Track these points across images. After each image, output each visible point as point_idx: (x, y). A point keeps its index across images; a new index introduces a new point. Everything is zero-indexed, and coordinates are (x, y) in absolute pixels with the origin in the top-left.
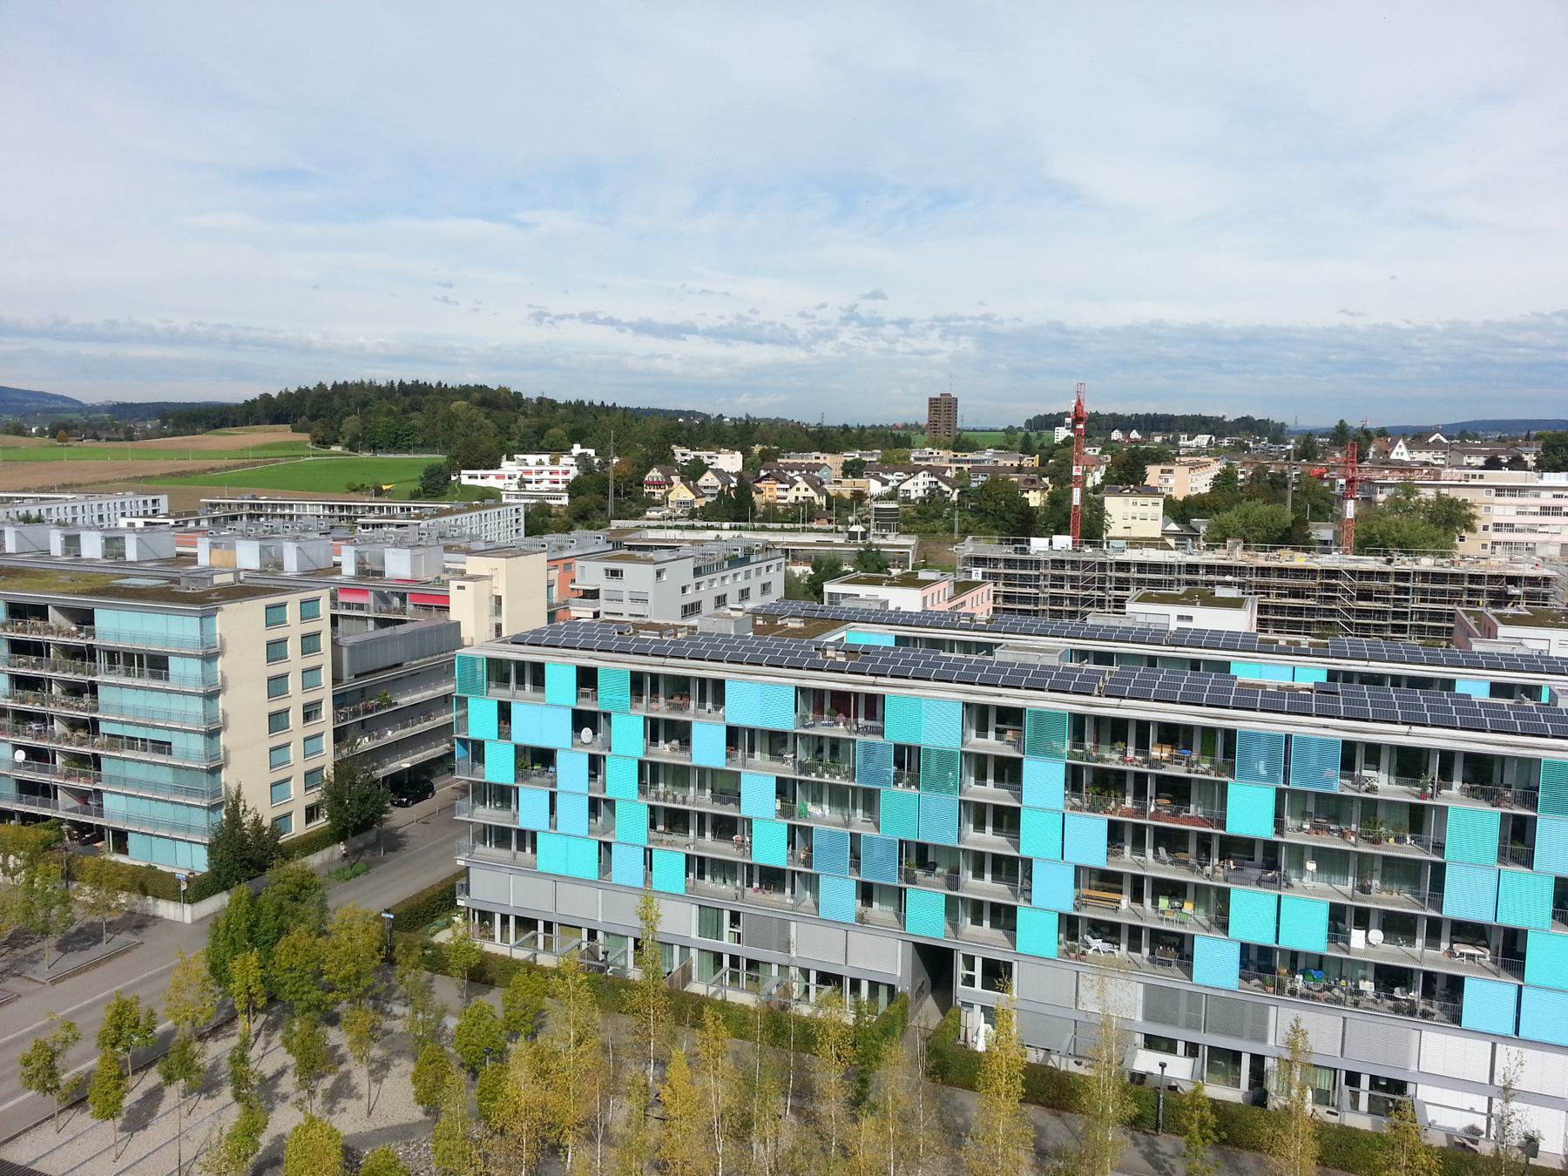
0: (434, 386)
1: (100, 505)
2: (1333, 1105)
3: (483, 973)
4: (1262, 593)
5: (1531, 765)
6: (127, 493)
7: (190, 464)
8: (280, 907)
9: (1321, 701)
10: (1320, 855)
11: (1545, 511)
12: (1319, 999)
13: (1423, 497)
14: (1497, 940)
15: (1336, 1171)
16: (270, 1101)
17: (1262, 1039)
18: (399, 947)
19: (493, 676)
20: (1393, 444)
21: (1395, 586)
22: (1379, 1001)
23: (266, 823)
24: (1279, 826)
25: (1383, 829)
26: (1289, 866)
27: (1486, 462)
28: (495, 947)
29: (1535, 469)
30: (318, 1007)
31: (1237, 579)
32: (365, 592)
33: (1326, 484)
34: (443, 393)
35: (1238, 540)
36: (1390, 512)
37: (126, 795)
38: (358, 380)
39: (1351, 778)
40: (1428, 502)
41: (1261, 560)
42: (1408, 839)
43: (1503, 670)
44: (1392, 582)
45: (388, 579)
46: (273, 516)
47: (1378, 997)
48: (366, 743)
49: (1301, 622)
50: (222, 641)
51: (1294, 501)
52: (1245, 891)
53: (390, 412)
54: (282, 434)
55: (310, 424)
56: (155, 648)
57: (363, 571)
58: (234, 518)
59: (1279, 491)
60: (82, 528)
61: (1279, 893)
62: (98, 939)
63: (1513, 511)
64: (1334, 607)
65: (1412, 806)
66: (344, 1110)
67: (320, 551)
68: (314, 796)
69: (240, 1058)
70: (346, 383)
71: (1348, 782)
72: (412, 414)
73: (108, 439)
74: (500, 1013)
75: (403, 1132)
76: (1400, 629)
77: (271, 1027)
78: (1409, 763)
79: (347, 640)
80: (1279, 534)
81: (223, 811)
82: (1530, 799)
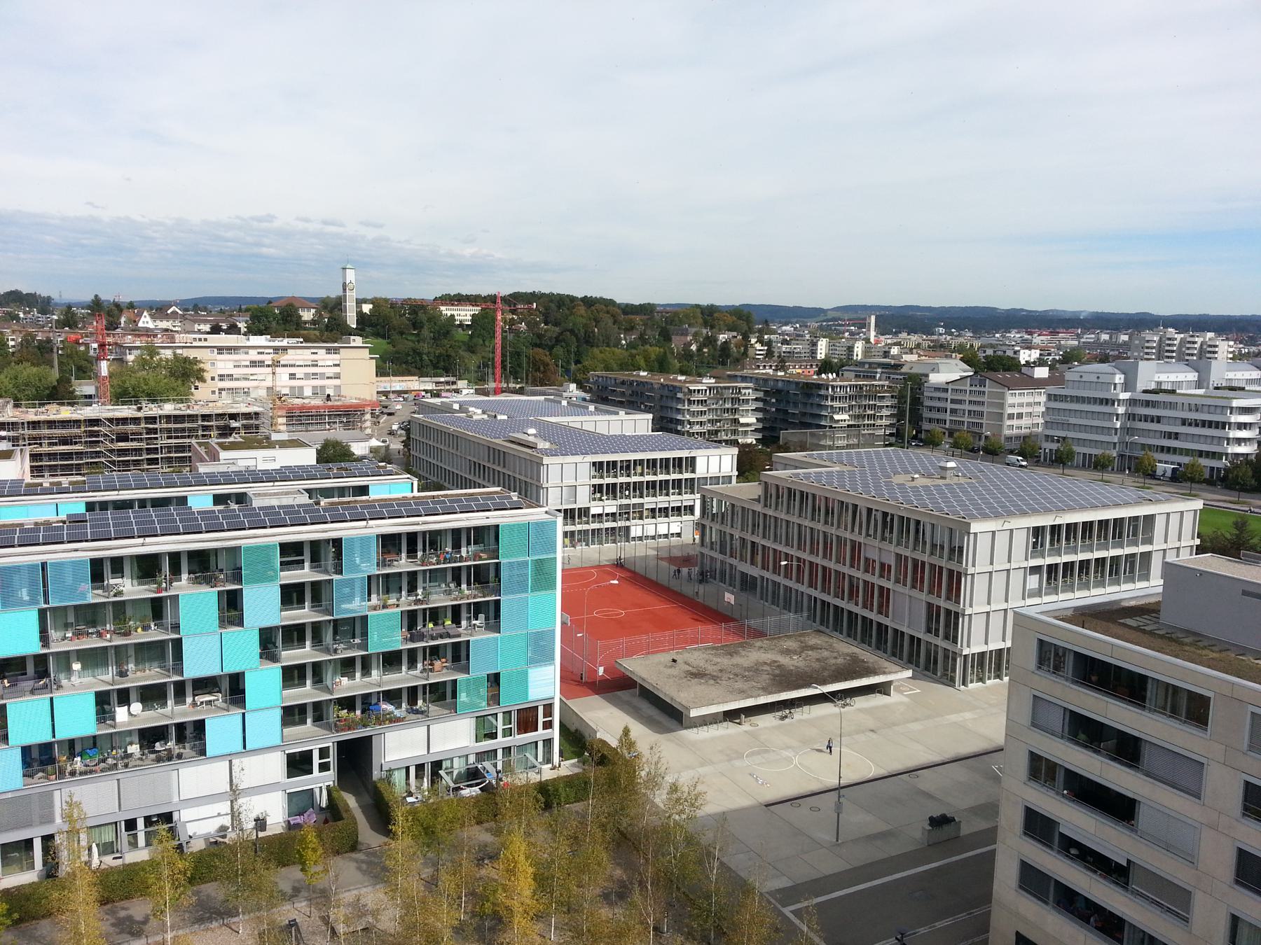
2: (117, 851)
4: (35, 444)
5: (235, 551)
9: (74, 529)
10: (84, 656)
11: (254, 364)
12: (96, 772)
13: (163, 356)
14: (225, 685)
15: (123, 902)
17: (49, 819)
20: (140, 315)
21: (146, 428)
22: (144, 757)
24: (44, 639)
25: (131, 623)
26: (58, 671)
27: (211, 328)
29: (245, 334)
31: (11, 434)
33: (82, 348)
35: (8, 399)
36: (139, 369)
39: (102, 587)
40: (167, 361)
41: (32, 415)
42: (152, 626)
43: (318, 479)
44: (143, 425)
47: (143, 755)
49: (72, 465)
51: (60, 363)
52: (21, 702)
59: (47, 355)
61: (51, 695)
63: (231, 365)
64: (98, 449)
65: (153, 600)
71: (100, 592)
76: (154, 461)
78: (147, 567)
80: (47, 392)
82: (237, 577)
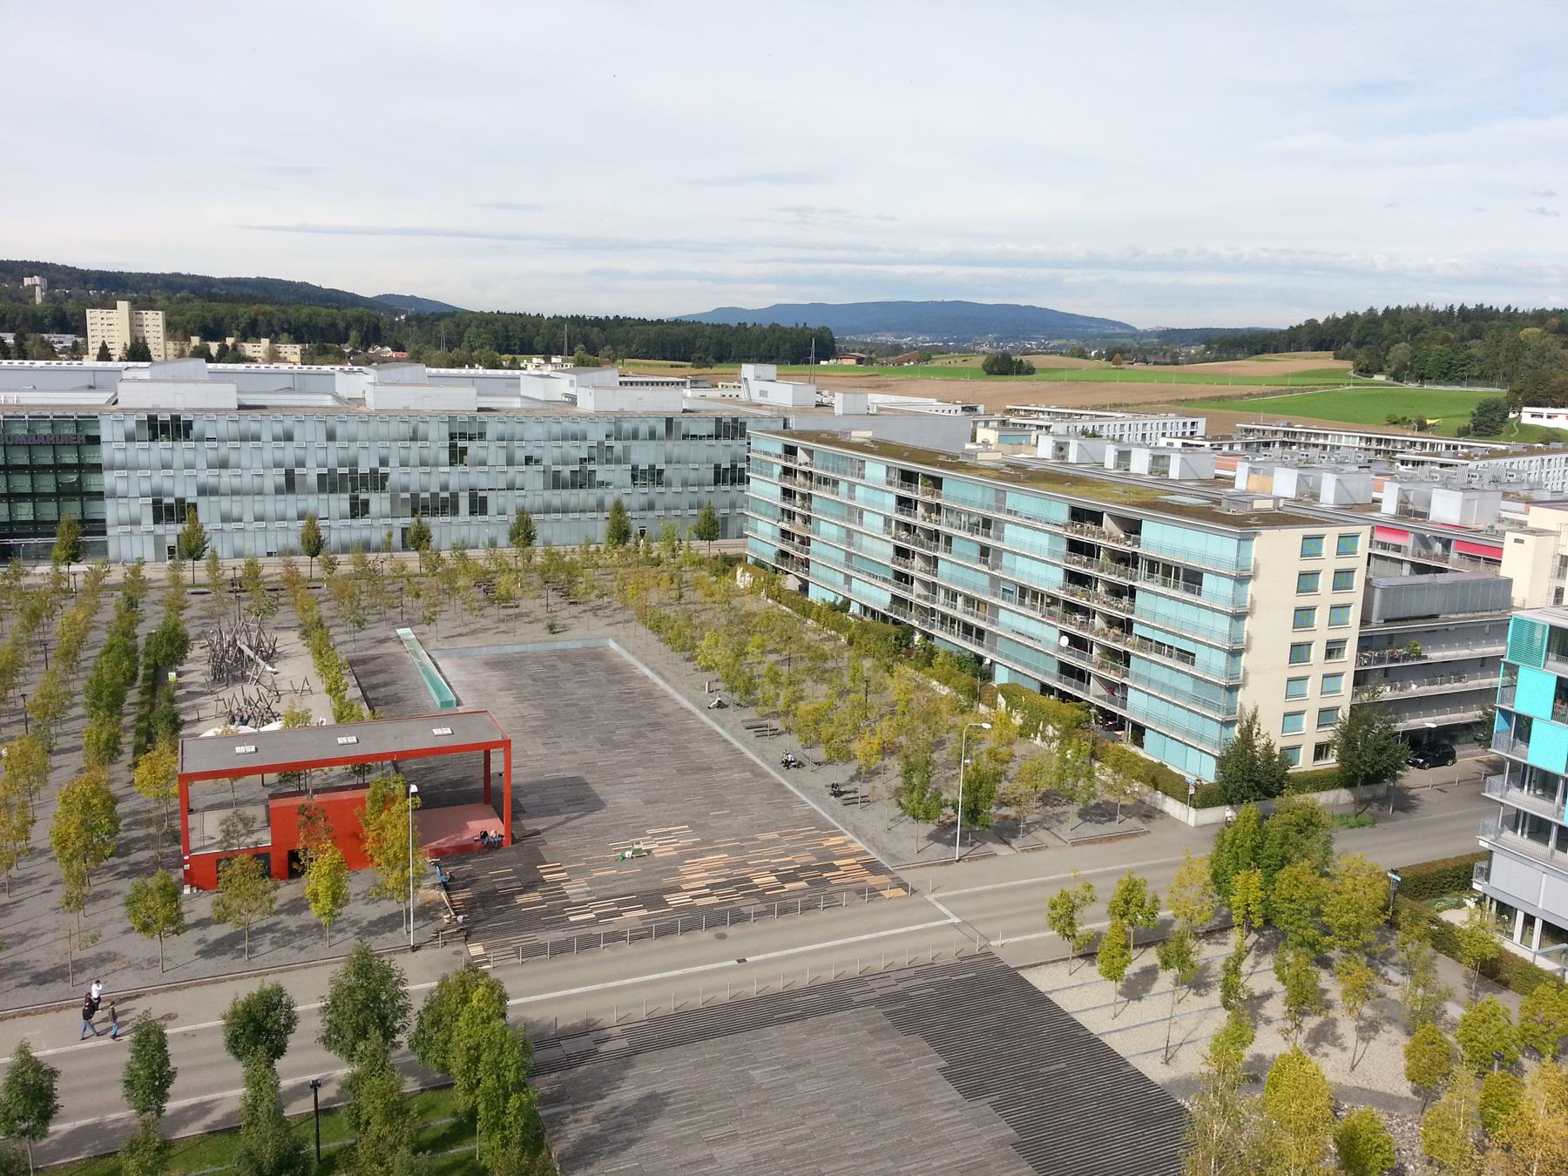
0: (1501, 310)
1: (1145, 425)
3: (1498, 971)
7: (1229, 389)
8: (1286, 837)
16: (1254, 1019)
18: (1405, 912)
19: (1555, 646)
23: (1277, 751)
28: (1513, 946)
30: (1312, 946)
32: (1404, 533)
34: (1512, 318)
37: (1149, 694)
38: (1413, 304)
45: (1433, 523)
46: (1307, 445)
48: (1387, 693)
50: (1257, 567)
53: (1446, 340)
54: (1324, 361)
55: (1356, 351)
56: (1193, 563)
57: (1405, 511)
58: (1267, 444)
60: (1133, 445)
66: (1326, 1055)
67: (1360, 485)
68: (1326, 735)
69: (1233, 969)
70: (1399, 307)
72: (1470, 343)
73: (1155, 363)
74: (1515, 1017)
75: (1389, 1102)
77: (1263, 949)
79: (1380, 582)
81: (1236, 728)
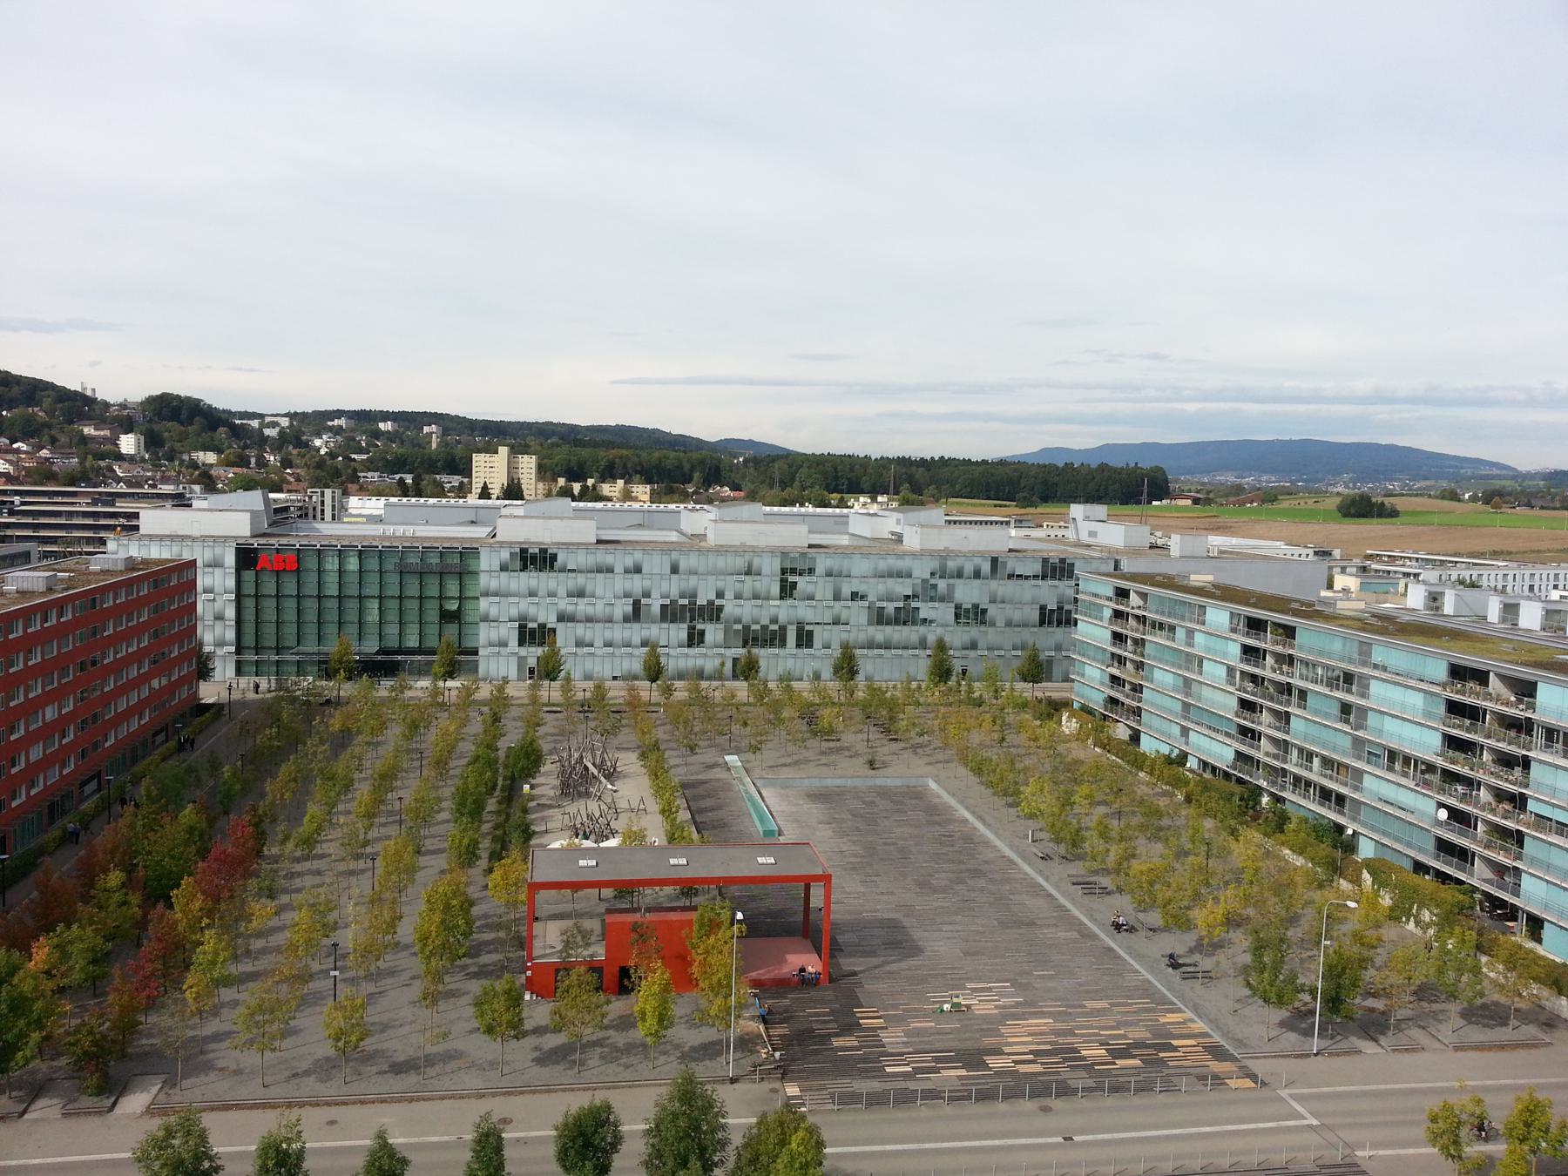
6: (1562, 565)
62: (1504, 1023)
73: (1542, 508)
